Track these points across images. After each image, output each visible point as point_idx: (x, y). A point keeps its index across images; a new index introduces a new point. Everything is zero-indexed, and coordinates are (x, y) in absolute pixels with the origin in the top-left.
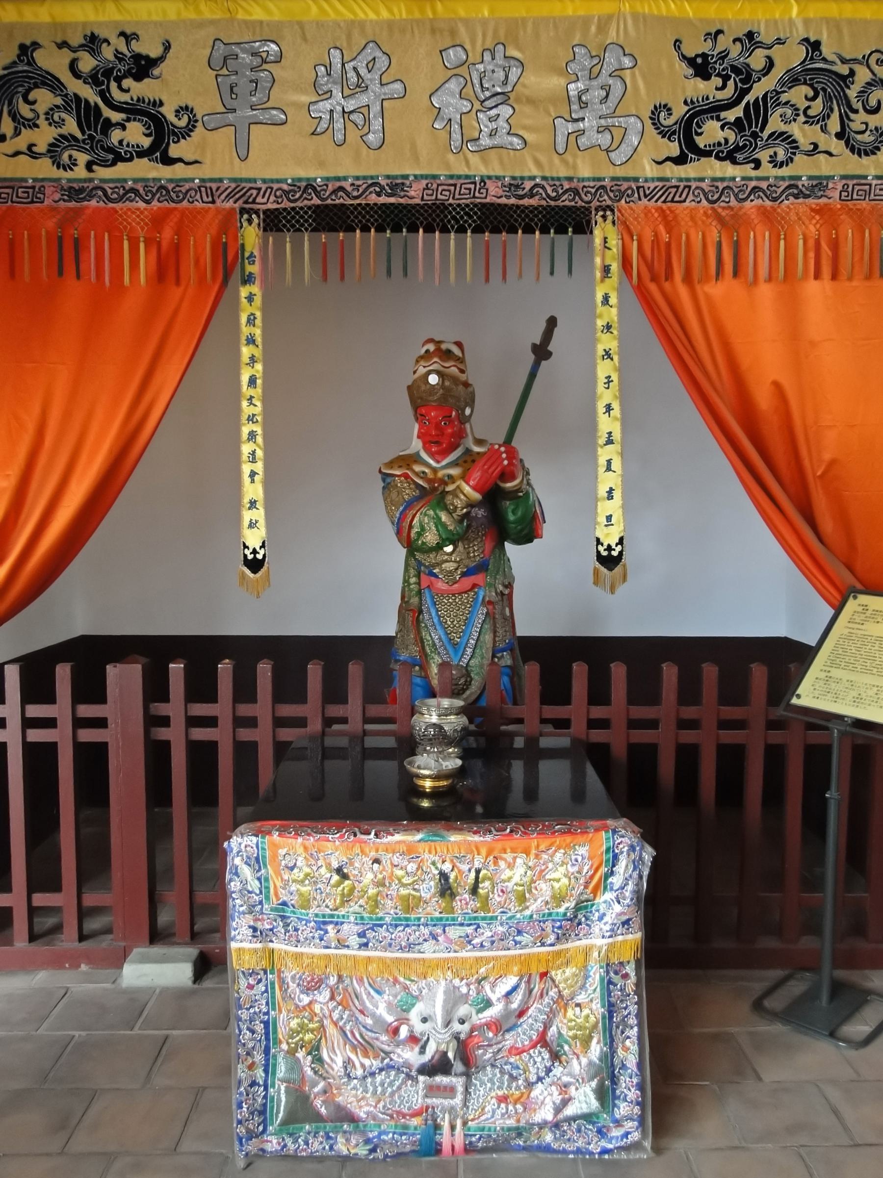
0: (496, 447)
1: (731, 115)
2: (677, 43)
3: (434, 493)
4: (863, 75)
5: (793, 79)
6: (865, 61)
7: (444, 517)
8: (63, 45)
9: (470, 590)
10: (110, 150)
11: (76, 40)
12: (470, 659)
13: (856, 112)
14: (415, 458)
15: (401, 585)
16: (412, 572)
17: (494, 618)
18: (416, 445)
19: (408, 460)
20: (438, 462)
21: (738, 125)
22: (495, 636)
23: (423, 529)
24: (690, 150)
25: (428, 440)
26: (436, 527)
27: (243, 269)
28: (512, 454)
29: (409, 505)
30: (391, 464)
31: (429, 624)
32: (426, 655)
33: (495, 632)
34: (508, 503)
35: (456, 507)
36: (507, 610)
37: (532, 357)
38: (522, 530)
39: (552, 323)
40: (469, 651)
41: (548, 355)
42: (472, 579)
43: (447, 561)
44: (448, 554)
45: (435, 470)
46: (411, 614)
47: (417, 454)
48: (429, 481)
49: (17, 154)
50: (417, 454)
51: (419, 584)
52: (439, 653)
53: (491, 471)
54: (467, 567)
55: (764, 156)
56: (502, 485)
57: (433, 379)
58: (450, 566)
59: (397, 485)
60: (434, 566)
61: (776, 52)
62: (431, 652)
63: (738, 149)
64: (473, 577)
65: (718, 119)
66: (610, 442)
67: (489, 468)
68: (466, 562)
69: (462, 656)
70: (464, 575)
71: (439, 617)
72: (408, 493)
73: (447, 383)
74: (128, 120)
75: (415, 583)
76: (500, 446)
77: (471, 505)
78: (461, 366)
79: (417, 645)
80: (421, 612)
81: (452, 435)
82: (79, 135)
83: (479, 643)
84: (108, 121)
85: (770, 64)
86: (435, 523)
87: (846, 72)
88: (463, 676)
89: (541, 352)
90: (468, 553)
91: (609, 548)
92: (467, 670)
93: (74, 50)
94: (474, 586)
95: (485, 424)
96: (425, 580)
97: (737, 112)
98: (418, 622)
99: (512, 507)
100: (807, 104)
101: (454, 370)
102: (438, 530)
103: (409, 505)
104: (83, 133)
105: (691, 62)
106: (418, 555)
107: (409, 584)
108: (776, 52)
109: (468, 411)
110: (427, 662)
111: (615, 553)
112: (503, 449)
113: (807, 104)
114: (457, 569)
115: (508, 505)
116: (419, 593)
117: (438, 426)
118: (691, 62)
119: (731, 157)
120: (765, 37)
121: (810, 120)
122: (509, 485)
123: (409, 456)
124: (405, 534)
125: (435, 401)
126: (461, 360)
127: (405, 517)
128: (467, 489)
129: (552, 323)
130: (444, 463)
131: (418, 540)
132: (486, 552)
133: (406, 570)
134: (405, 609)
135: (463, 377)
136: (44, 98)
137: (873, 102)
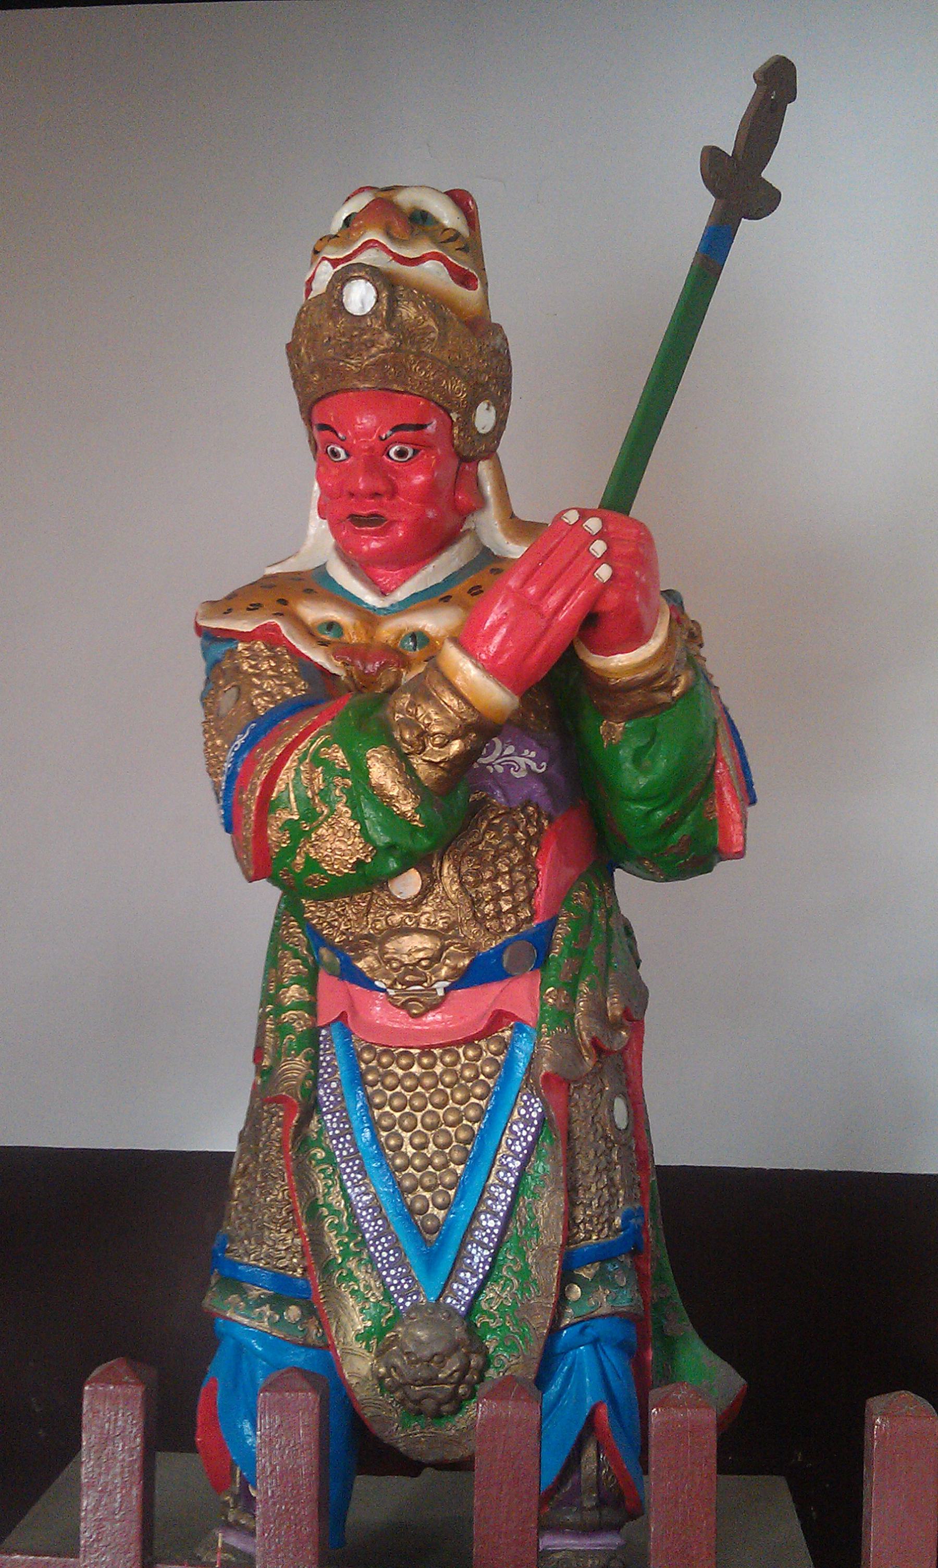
0: (572, 517)
3: (361, 694)
7: (380, 771)
9: (485, 1034)
12: (482, 1285)
14: (316, 584)
15: (256, 1011)
16: (291, 966)
17: (569, 1137)
18: (317, 543)
19: (280, 592)
20: (383, 593)
22: (571, 1203)
23: (310, 814)
25: (350, 516)
26: (354, 805)
28: (635, 553)
29: (265, 728)
30: (227, 605)
31: (342, 1149)
32: (327, 1267)
33: (571, 1190)
34: (620, 727)
35: (423, 734)
36: (620, 1106)
37: (708, 201)
38: (670, 825)
39: (777, 85)
40: (478, 1256)
41: (766, 201)
42: (487, 998)
43: (403, 930)
44: (402, 906)
45: (370, 618)
46: (286, 1112)
47: (321, 572)
48: (345, 652)
50: (321, 572)
51: (312, 1007)
52: (372, 1260)
53: (553, 601)
54: (471, 951)
56: (596, 661)
57: (360, 297)
58: (415, 946)
59: (238, 669)
60: (359, 945)
62: (345, 1254)
64: (495, 989)
67: (545, 592)
68: (471, 931)
69: (452, 1276)
70: (463, 979)
71: (375, 1126)
72: (269, 688)
73: (408, 312)
75: (296, 1007)
76: (584, 514)
77: (482, 730)
78: (463, 262)
79: (293, 1226)
80: (312, 1107)
81: (429, 494)
83: (515, 1226)
86: (347, 791)
88: (456, 1348)
89: (739, 184)
90: (475, 903)
92: (471, 1328)
94: (498, 1019)
95: (543, 462)
96: (333, 995)
98: (301, 1139)
99: (637, 742)
101: (433, 273)
102: (358, 818)
103: (265, 728)
106: (311, 909)
107: (280, 1008)
109: (484, 418)
110: (330, 1289)
112: (593, 524)
114: (435, 959)
115: (616, 735)
116: (312, 1038)
117: (374, 461)
122: (620, 661)
123: (296, 578)
124: (248, 831)
125: (363, 374)
126: (471, 245)
127: (251, 765)
128: (467, 671)
129: (777, 85)
130: (401, 594)
131: (291, 851)
132: (540, 900)
133: (273, 962)
134: (265, 1096)
135: (469, 297)
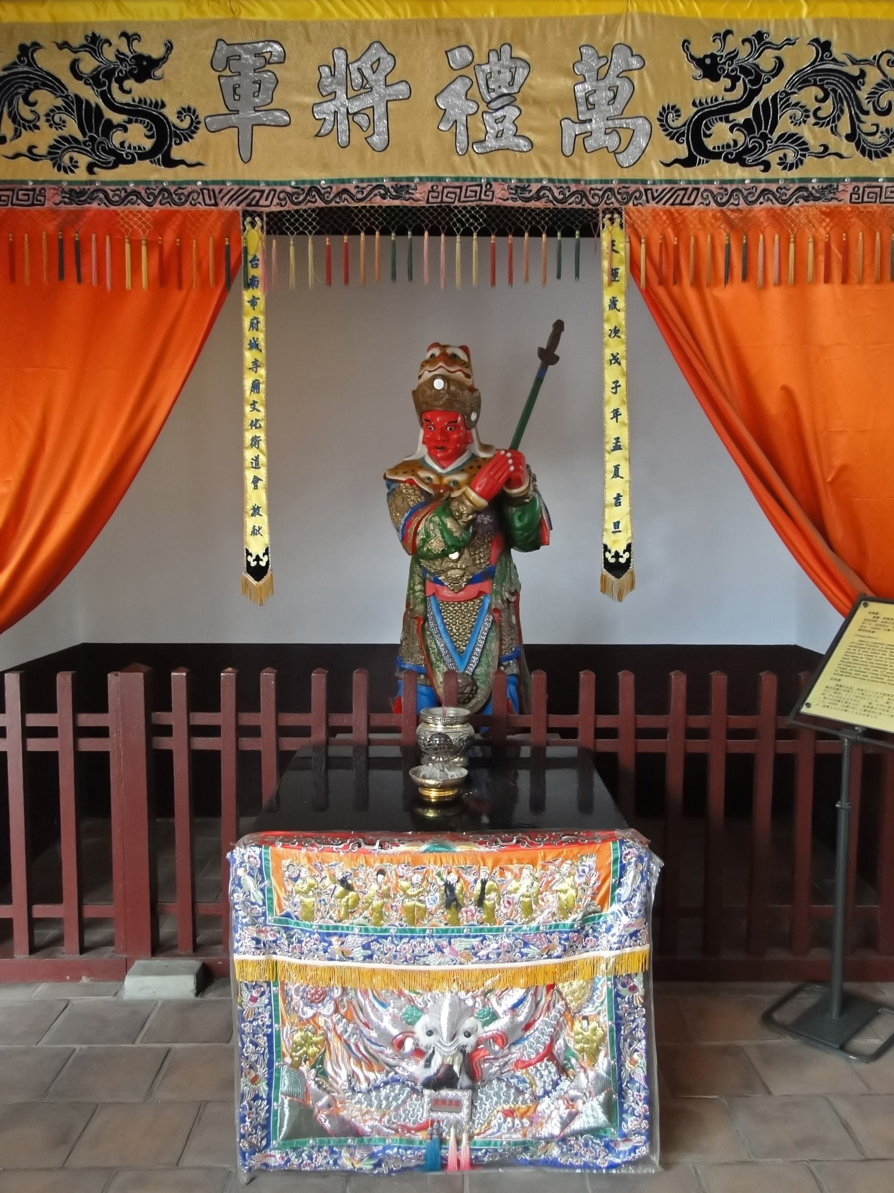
0: (503, 452)
1: (740, 117)
2: (686, 44)
3: (439, 500)
4: (874, 76)
5: (803, 80)
6: (876, 62)
7: (449, 524)
8: (64, 45)
9: (476, 598)
10: (111, 152)
11: (77, 40)
12: (476, 667)
13: (867, 113)
14: (420, 464)
15: (406, 592)
16: (417, 579)
17: (500, 626)
18: (422, 451)
19: (413, 466)
20: (443, 468)
21: (747, 126)
22: (501, 644)
23: (428, 535)
24: (699, 152)
25: (433, 445)
26: (442, 533)
27: (246, 272)
28: (518, 459)
29: (414, 511)
30: (395, 470)
31: (434, 632)
32: (431, 663)
33: (501, 640)
34: (514, 509)
35: (462, 514)
36: (514, 618)
37: (539, 361)
38: (528, 537)
39: (559, 327)
40: (475, 659)
41: (555, 360)
42: (478, 587)
43: (452, 568)
44: (453, 561)
45: (440, 476)
46: (416, 621)
47: (423, 460)
48: (434, 487)
49: (17, 155)
50: (423, 460)
51: (424, 591)
52: (444, 662)
53: (497, 477)
54: (473, 574)
55: (773, 158)
56: (509, 491)
57: (439, 384)
58: (456, 573)
59: (401, 492)
60: (440, 573)
61: (786, 53)
62: (437, 660)
63: (747, 151)
64: (479, 585)
65: (727, 120)
66: (617, 447)
67: (495, 474)
68: (472, 569)
69: (468, 665)
70: (469, 582)
71: (445, 624)
72: (414, 499)
73: (453, 388)
74: (130, 121)
75: (420, 591)
76: (506, 451)
77: (477, 511)
78: (467, 371)
79: (422, 653)
80: (426, 620)
81: (458, 440)
82: (80, 137)
83: (485, 651)
84: (109, 122)
85: (780, 65)
86: (440, 530)
87: (856, 73)
88: (468, 685)
89: (548, 356)
90: (474, 560)
91: (617, 555)
92: (473, 679)
93: (75, 51)
94: (480, 593)
95: (491, 430)
96: (431, 587)
97: (747, 113)
98: (423, 630)
99: (519, 513)
100: (817, 105)
101: (460, 375)
102: (443, 537)
103: (414, 511)
104: (84, 135)
105: (700, 63)
106: (424, 563)
107: (414, 592)
108: (786, 53)
109: (474, 417)
110: (433, 670)
111: (622, 560)
112: (509, 455)
113: (817, 105)
114: (462, 576)
115: (514, 512)
116: (425, 601)
117: (443, 431)
118: (699, 63)
119: (740, 159)
120: (775, 37)
121: (820, 122)
122: (515, 491)
123: (415, 462)
124: (410, 541)
125: (440, 406)
126: (467, 365)
127: (410, 523)
128: (473, 495)
129: (559, 327)
130: (449, 469)
131: (423, 547)
132: (492, 559)
133: (411, 577)
134: (410, 616)
135: (469, 382)
136: (45, 100)
137: (884, 104)
